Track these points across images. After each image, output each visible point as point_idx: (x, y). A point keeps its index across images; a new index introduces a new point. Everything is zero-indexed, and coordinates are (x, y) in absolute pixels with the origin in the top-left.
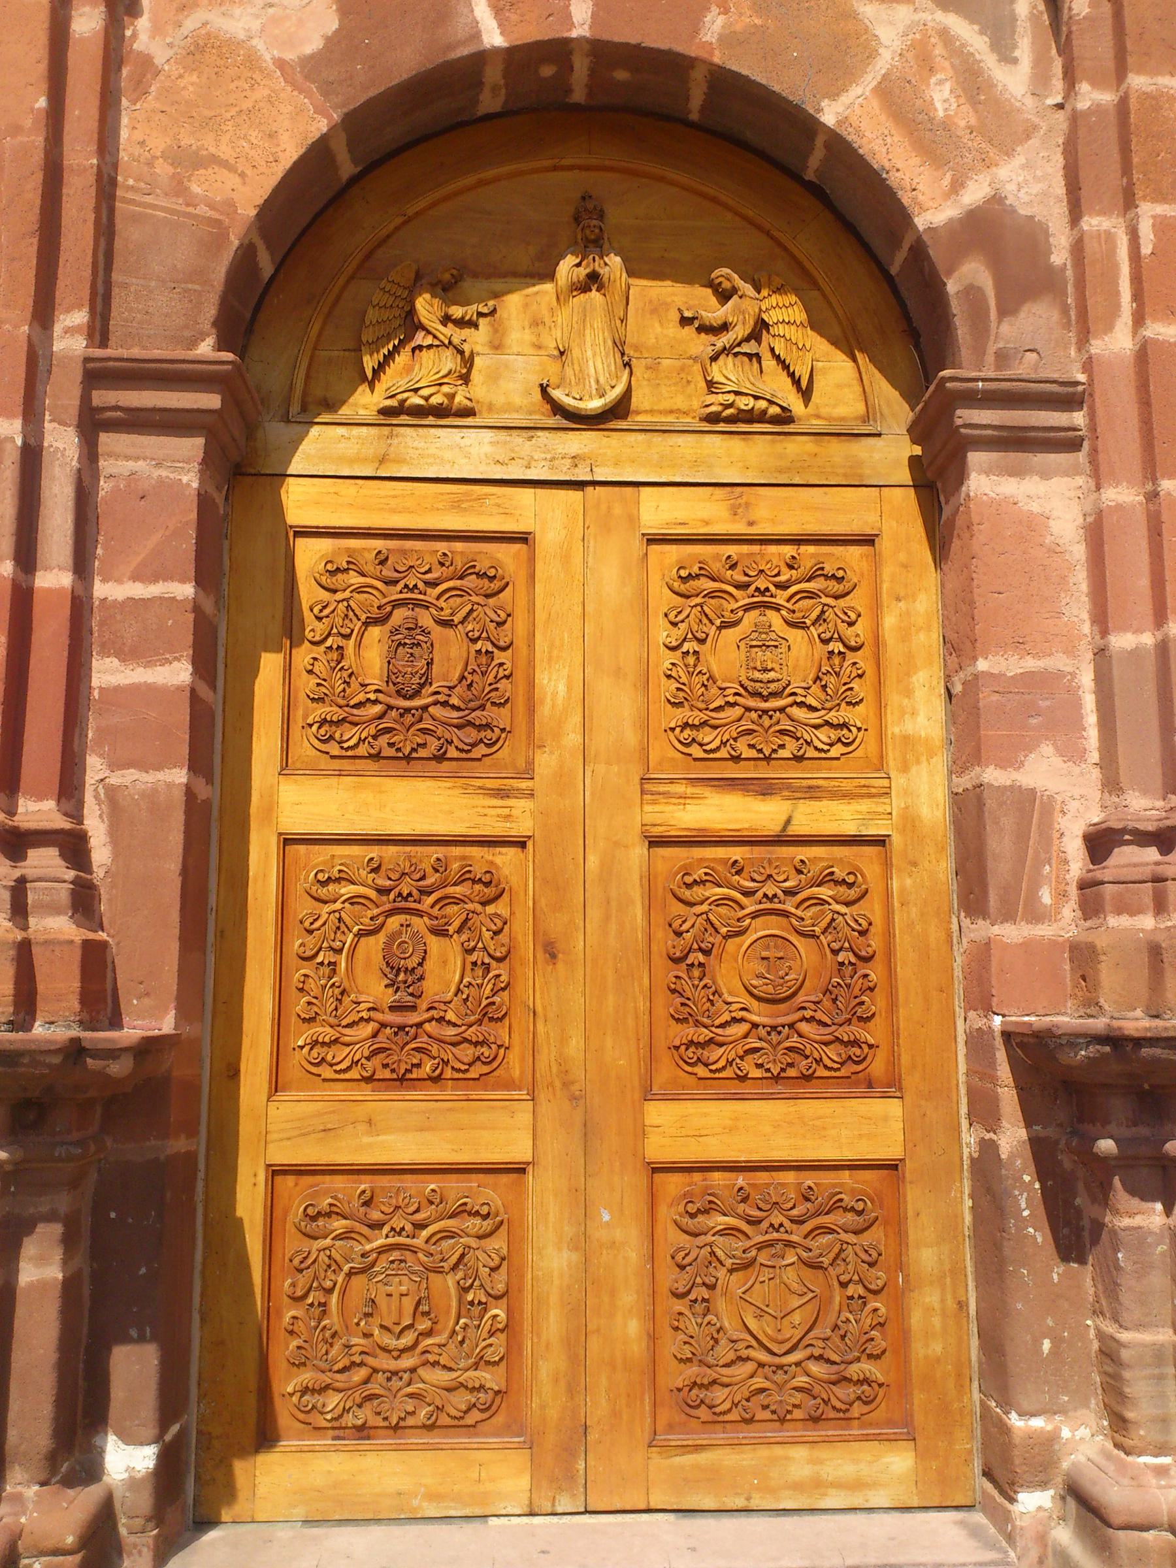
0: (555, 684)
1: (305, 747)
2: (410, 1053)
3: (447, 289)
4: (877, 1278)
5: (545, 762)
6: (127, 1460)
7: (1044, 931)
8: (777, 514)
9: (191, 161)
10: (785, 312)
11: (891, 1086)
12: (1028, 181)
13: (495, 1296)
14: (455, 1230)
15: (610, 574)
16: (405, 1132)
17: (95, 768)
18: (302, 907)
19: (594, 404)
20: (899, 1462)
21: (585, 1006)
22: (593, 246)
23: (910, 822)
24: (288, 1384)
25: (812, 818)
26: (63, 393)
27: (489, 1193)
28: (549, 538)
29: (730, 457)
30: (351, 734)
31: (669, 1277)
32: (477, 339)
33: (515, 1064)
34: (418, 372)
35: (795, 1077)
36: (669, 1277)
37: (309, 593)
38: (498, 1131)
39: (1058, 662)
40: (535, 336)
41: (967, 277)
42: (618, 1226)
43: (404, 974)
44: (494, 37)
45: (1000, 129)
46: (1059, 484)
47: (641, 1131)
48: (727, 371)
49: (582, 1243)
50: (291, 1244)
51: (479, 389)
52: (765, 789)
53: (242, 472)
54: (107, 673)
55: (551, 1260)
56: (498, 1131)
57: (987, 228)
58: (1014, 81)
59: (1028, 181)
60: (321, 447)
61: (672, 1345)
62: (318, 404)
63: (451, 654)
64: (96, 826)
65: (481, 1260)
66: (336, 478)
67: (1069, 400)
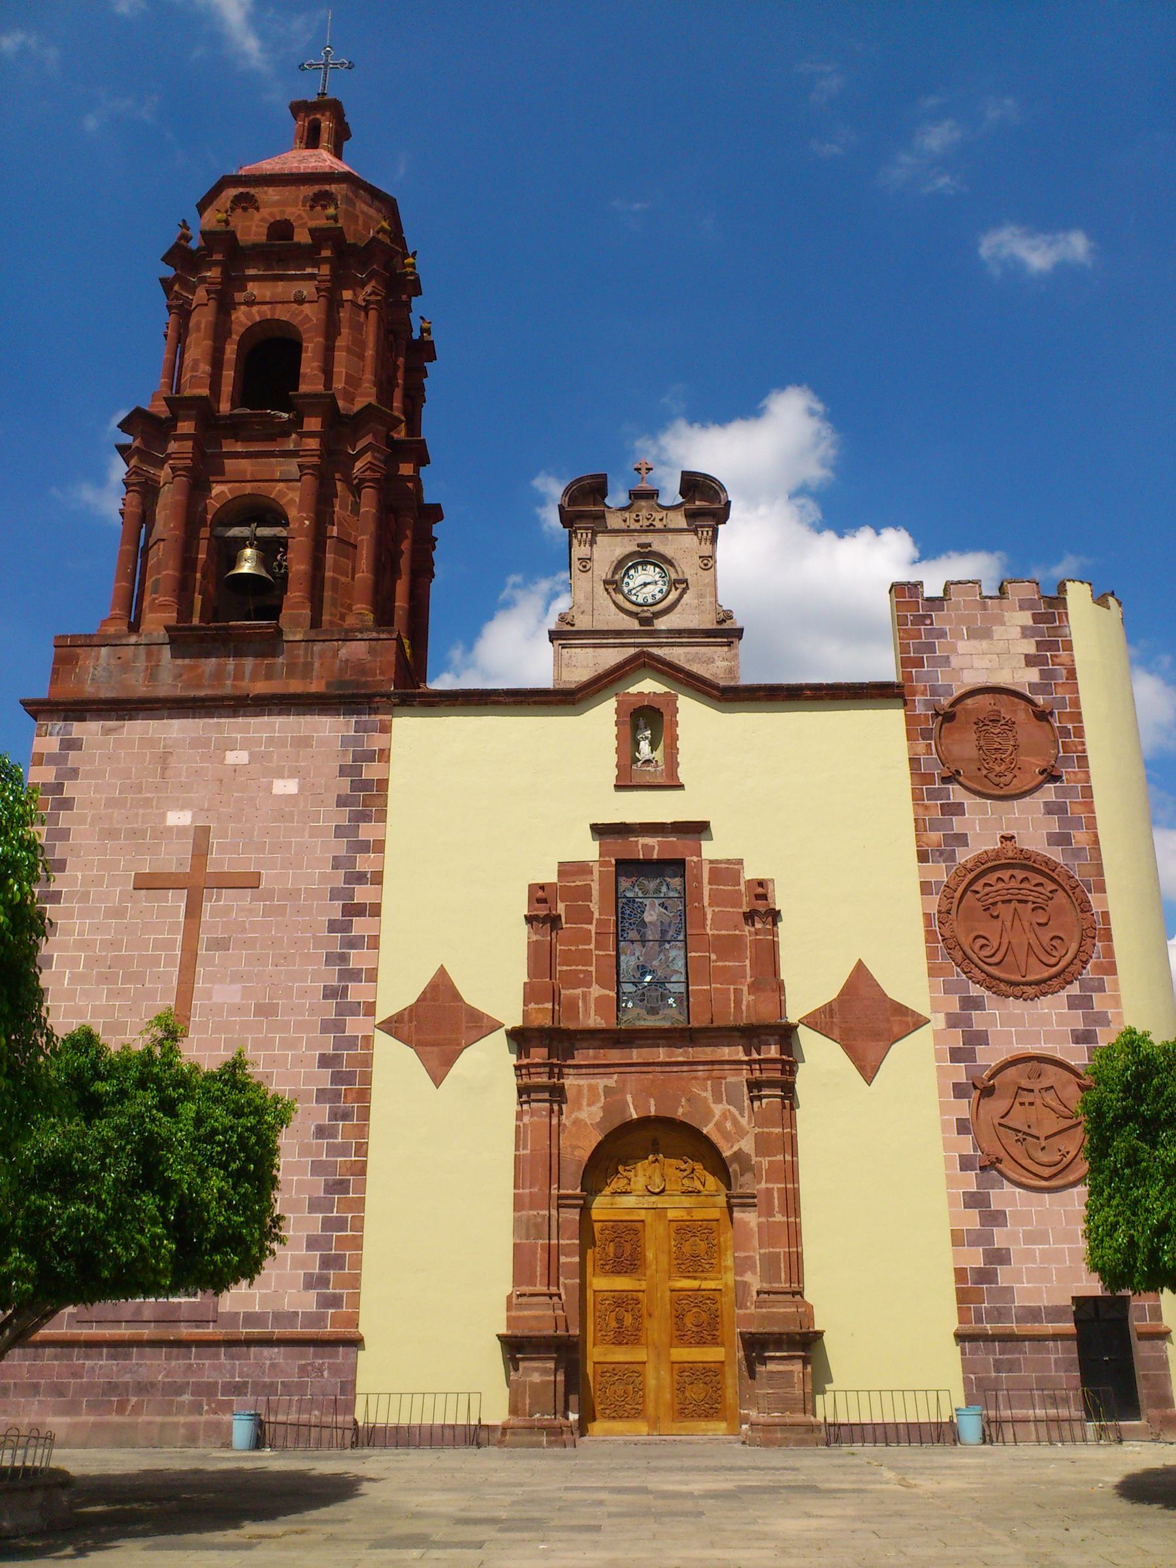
0: (650, 1255)
1: (598, 1270)
2: (624, 1337)
3: (625, 1164)
4: (719, 1386)
5: (648, 1273)
6: (573, 1417)
7: (748, 1311)
8: (698, 1215)
9: (574, 1147)
10: (698, 1166)
11: (722, 1345)
12: (747, 1145)
13: (641, 1389)
14: (632, 1373)
15: (661, 1230)
16: (620, 1355)
17: (562, 1279)
18: (599, 1307)
19: (657, 1190)
20: (723, 1425)
21: (657, 1328)
22: (656, 1152)
23: (726, 1285)
24: (598, 1408)
25: (707, 1285)
26: (554, 1203)
27: (637, 1367)
28: (649, 1221)
29: (687, 1201)
30: (607, 1267)
31: (676, 1386)
32: (632, 1174)
33: (643, 1340)
34: (617, 1184)
35: (702, 1343)
36: (676, 1386)
37: (597, 1235)
38: (640, 1354)
39: (752, 1254)
40: (642, 1174)
41: (734, 1168)
42: (665, 1374)
43: (620, 1320)
44: (635, 1116)
45: (741, 1133)
46: (753, 1214)
47: (669, 1354)
48: (686, 1181)
49: (658, 1379)
50: (599, 1378)
51: (632, 1186)
52: (695, 1278)
53: (585, 1210)
54: (563, 1259)
55: (651, 1382)
56: (640, 1354)
57: (739, 1156)
58: (744, 1121)
59: (747, 1145)
60: (599, 1202)
61: (677, 1400)
62: (597, 1191)
63: (628, 1248)
64: (562, 1291)
65: (637, 1381)
66: (602, 1207)
67: (754, 1197)
